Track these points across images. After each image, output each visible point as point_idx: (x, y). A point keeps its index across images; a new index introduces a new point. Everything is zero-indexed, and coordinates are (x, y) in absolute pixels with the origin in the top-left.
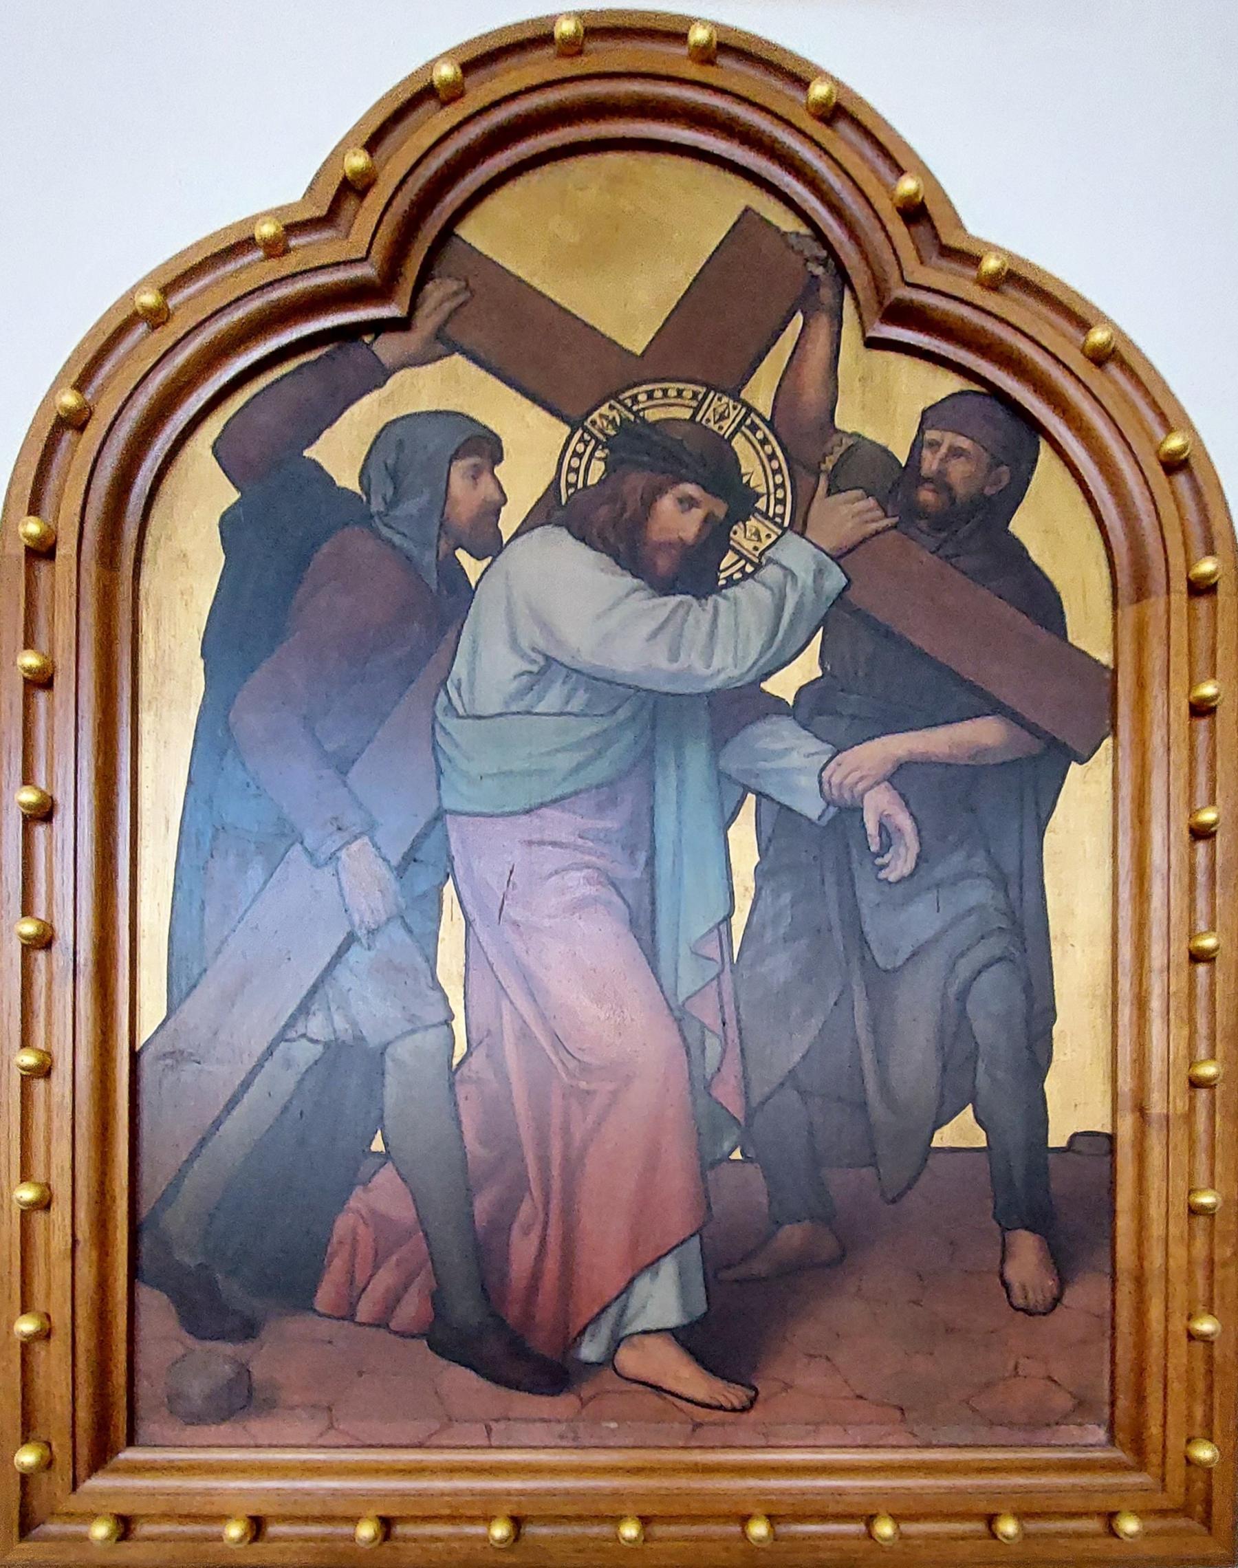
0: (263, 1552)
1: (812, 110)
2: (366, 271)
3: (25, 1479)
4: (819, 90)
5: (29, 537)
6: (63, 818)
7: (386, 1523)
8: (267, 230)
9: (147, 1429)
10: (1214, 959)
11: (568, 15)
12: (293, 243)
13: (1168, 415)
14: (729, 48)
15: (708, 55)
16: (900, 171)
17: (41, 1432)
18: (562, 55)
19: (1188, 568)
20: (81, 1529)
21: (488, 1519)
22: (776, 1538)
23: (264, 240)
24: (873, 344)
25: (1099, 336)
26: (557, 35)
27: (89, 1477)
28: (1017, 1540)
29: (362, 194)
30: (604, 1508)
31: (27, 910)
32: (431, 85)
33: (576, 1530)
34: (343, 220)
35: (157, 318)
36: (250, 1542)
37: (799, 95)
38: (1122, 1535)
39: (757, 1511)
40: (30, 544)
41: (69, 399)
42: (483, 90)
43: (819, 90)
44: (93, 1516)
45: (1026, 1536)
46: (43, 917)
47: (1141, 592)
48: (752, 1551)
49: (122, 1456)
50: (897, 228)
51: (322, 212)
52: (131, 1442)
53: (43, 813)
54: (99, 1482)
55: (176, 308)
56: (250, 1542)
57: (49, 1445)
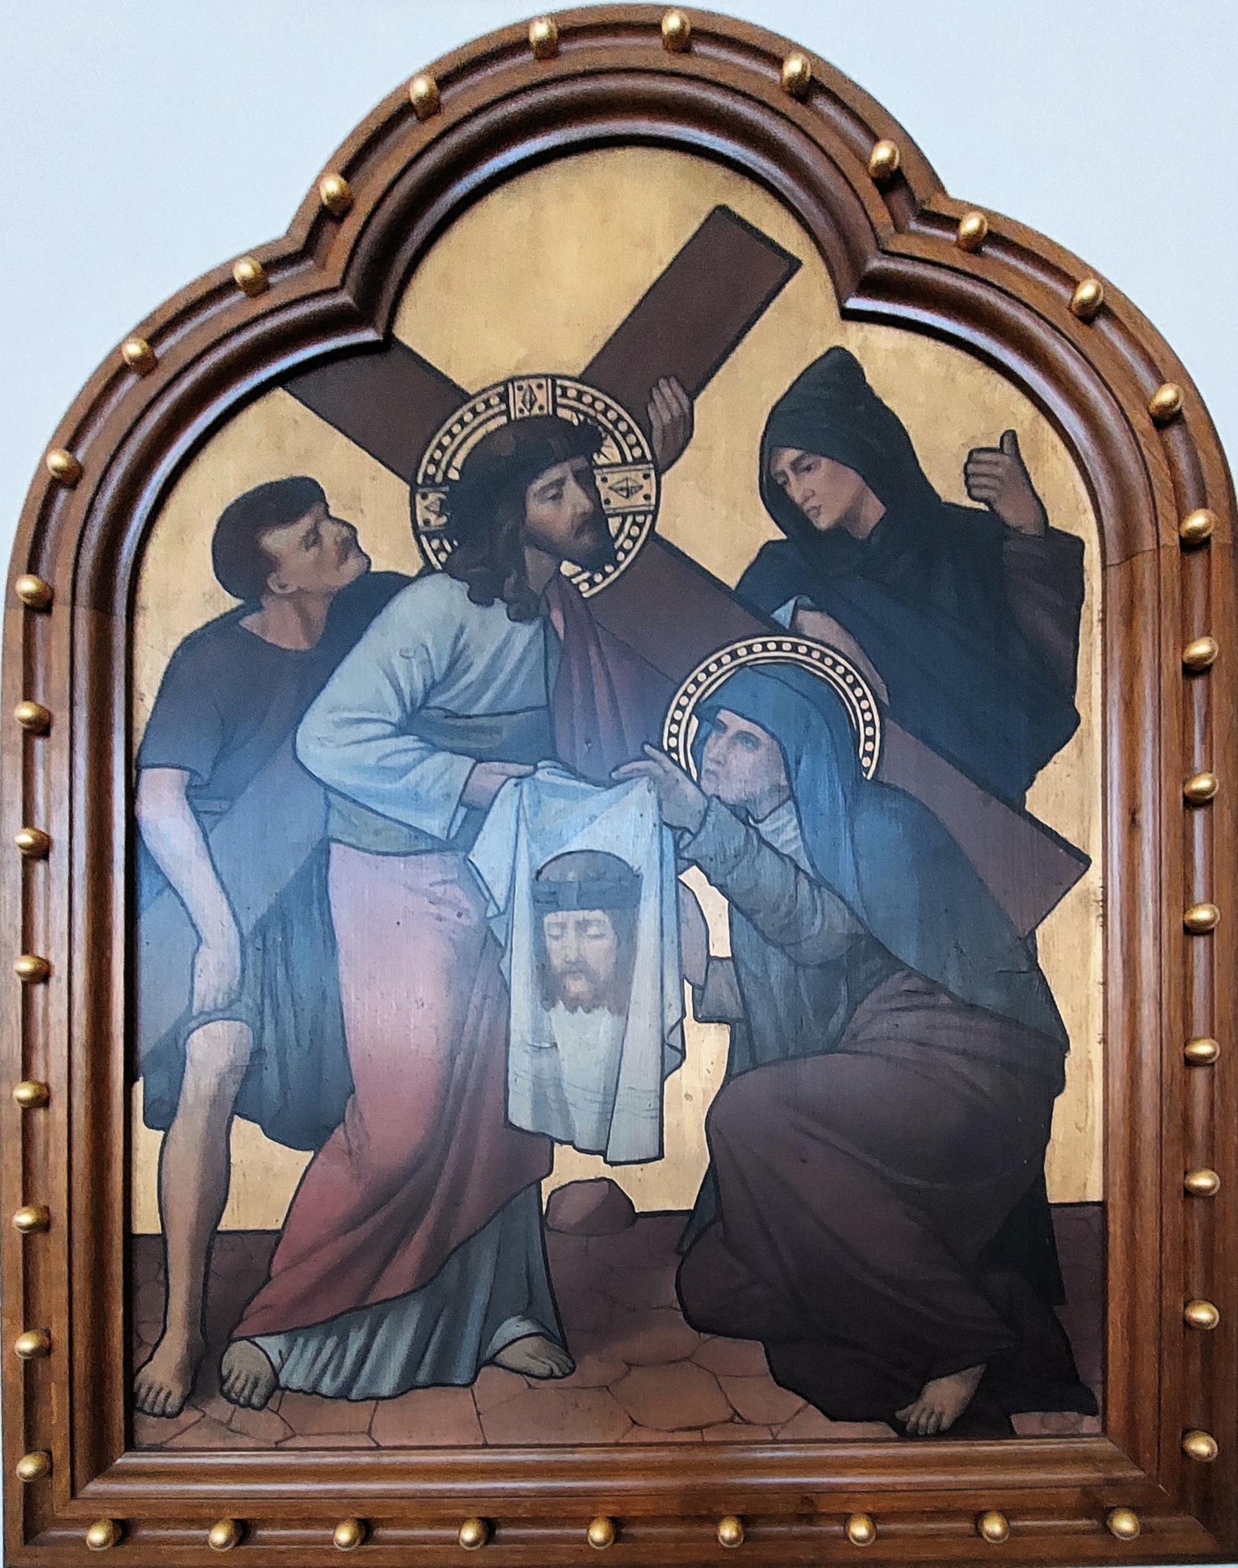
1: (788, 89)
2: (345, 298)
5: (27, 595)
6: (59, 856)
8: (244, 270)
10: (1212, 930)
11: (540, 18)
12: (272, 280)
14: (701, 33)
15: (682, 43)
17: (39, 1443)
20: (706, 1530)
22: (880, 1536)
24: (849, 315)
27: (88, 1482)
28: (1137, 1534)
31: (27, 949)
32: (410, 104)
34: (320, 249)
35: (145, 365)
36: (237, 1545)
37: (771, 73)
40: (28, 601)
42: (460, 99)
44: (90, 1522)
46: (41, 954)
49: (119, 1461)
52: (131, 1445)
54: (97, 1487)
55: (163, 357)
56: (237, 1545)
57: (50, 1453)
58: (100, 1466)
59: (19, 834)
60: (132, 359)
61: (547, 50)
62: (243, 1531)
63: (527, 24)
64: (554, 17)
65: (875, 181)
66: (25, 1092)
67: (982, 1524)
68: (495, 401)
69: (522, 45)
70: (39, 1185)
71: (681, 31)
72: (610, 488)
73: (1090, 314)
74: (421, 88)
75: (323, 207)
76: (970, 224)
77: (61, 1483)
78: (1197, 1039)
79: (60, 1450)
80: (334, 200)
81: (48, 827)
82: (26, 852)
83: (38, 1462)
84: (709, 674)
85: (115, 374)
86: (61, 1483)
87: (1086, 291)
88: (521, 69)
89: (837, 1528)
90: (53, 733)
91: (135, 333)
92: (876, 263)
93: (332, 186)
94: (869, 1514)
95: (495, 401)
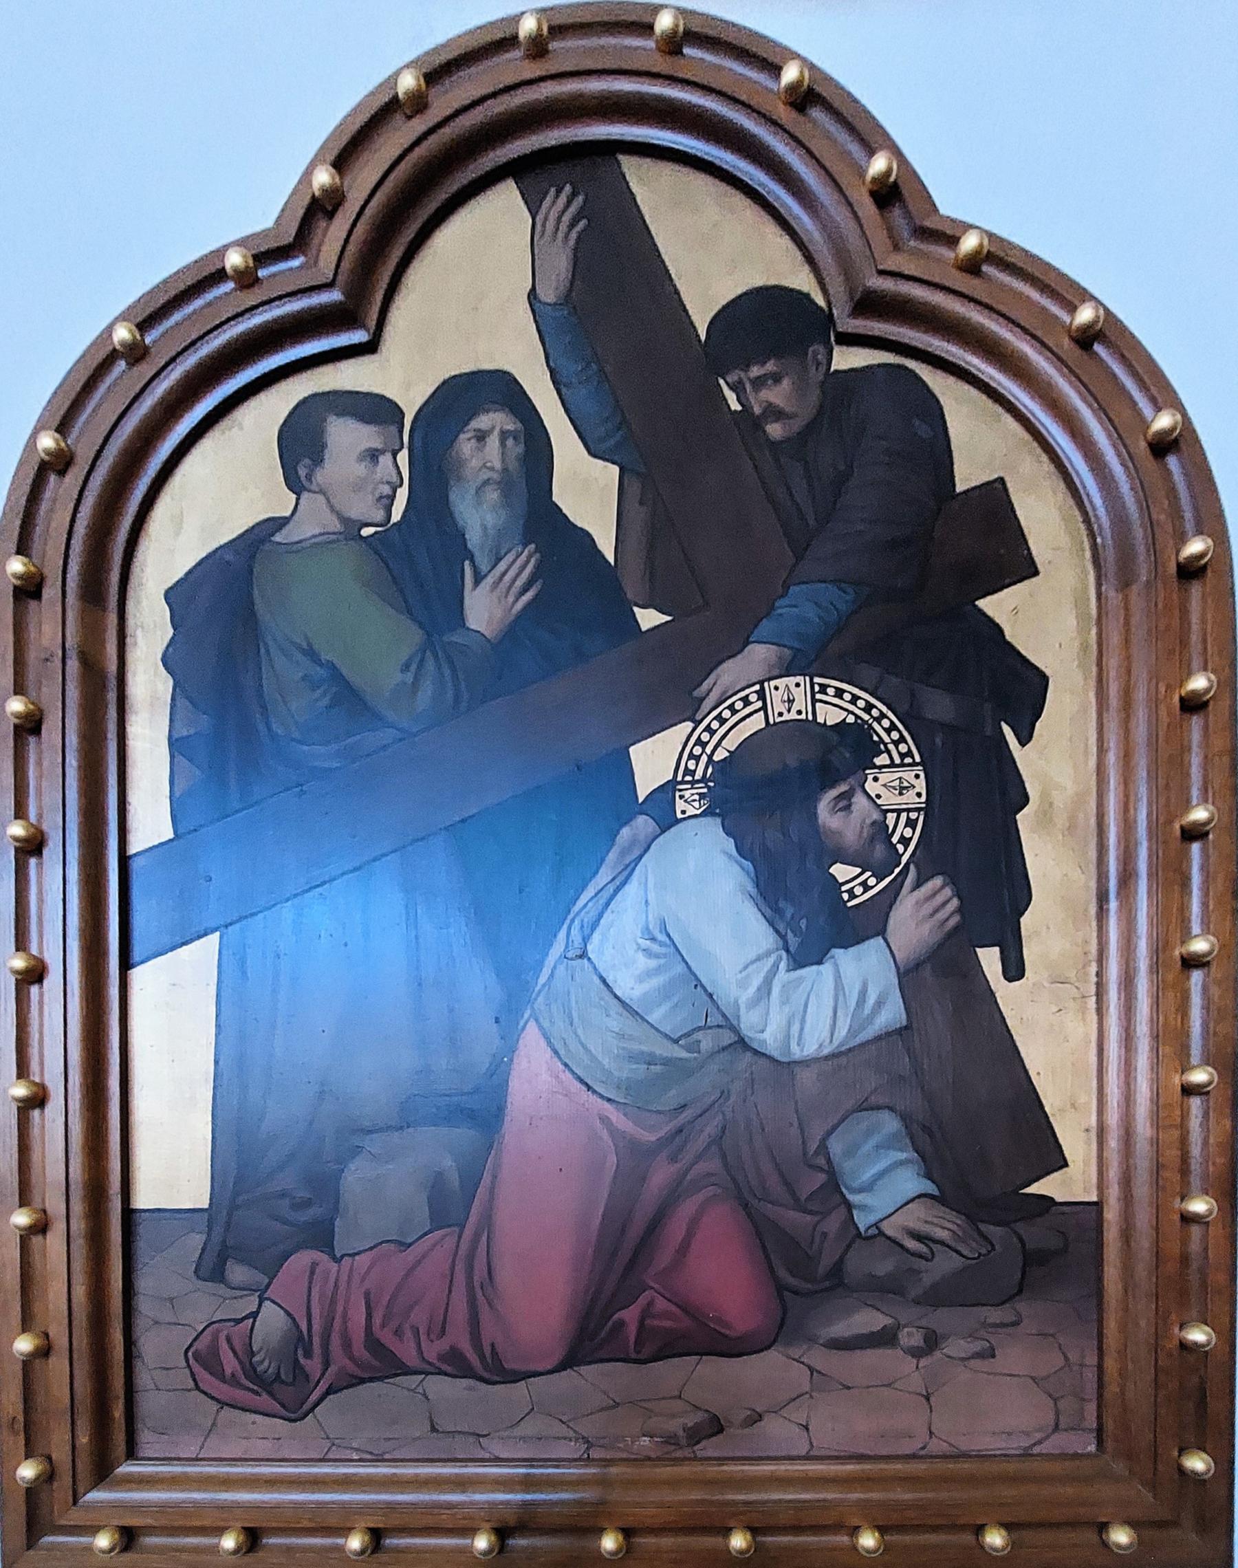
2: (335, 296)
3: (32, 1492)
5: (15, 576)
7: (376, 1536)
8: (234, 259)
9: (148, 1441)
12: (262, 273)
13: (1068, 293)
14: (700, 34)
16: (871, 152)
20: (213, 1541)
21: (471, 1531)
23: (236, 270)
29: (331, 215)
30: (333, 1521)
33: (933, 1538)
35: (135, 353)
40: (18, 583)
42: (444, 101)
43: (790, 74)
51: (289, 238)
52: (131, 1453)
53: (32, 847)
58: (102, 1473)
59: (13, 1085)
60: (123, 344)
61: (247, 280)
62: (252, 1538)
63: (516, 19)
65: (873, 194)
66: (22, 1218)
67: (983, 1536)
68: (753, 697)
69: (509, 42)
70: (37, 1307)
71: (674, 31)
72: (884, 785)
73: (1086, 338)
74: (408, 82)
75: (314, 199)
76: (969, 243)
77: (64, 1481)
78: (1194, 1067)
79: (61, 1455)
80: (324, 190)
81: (41, 952)
82: (19, 977)
83: (36, 1342)
84: (734, 712)
85: (209, 276)
86: (64, 1481)
87: (1085, 315)
89: (845, 1539)
90: (45, 852)
91: (123, 317)
93: (323, 177)
95: (753, 697)
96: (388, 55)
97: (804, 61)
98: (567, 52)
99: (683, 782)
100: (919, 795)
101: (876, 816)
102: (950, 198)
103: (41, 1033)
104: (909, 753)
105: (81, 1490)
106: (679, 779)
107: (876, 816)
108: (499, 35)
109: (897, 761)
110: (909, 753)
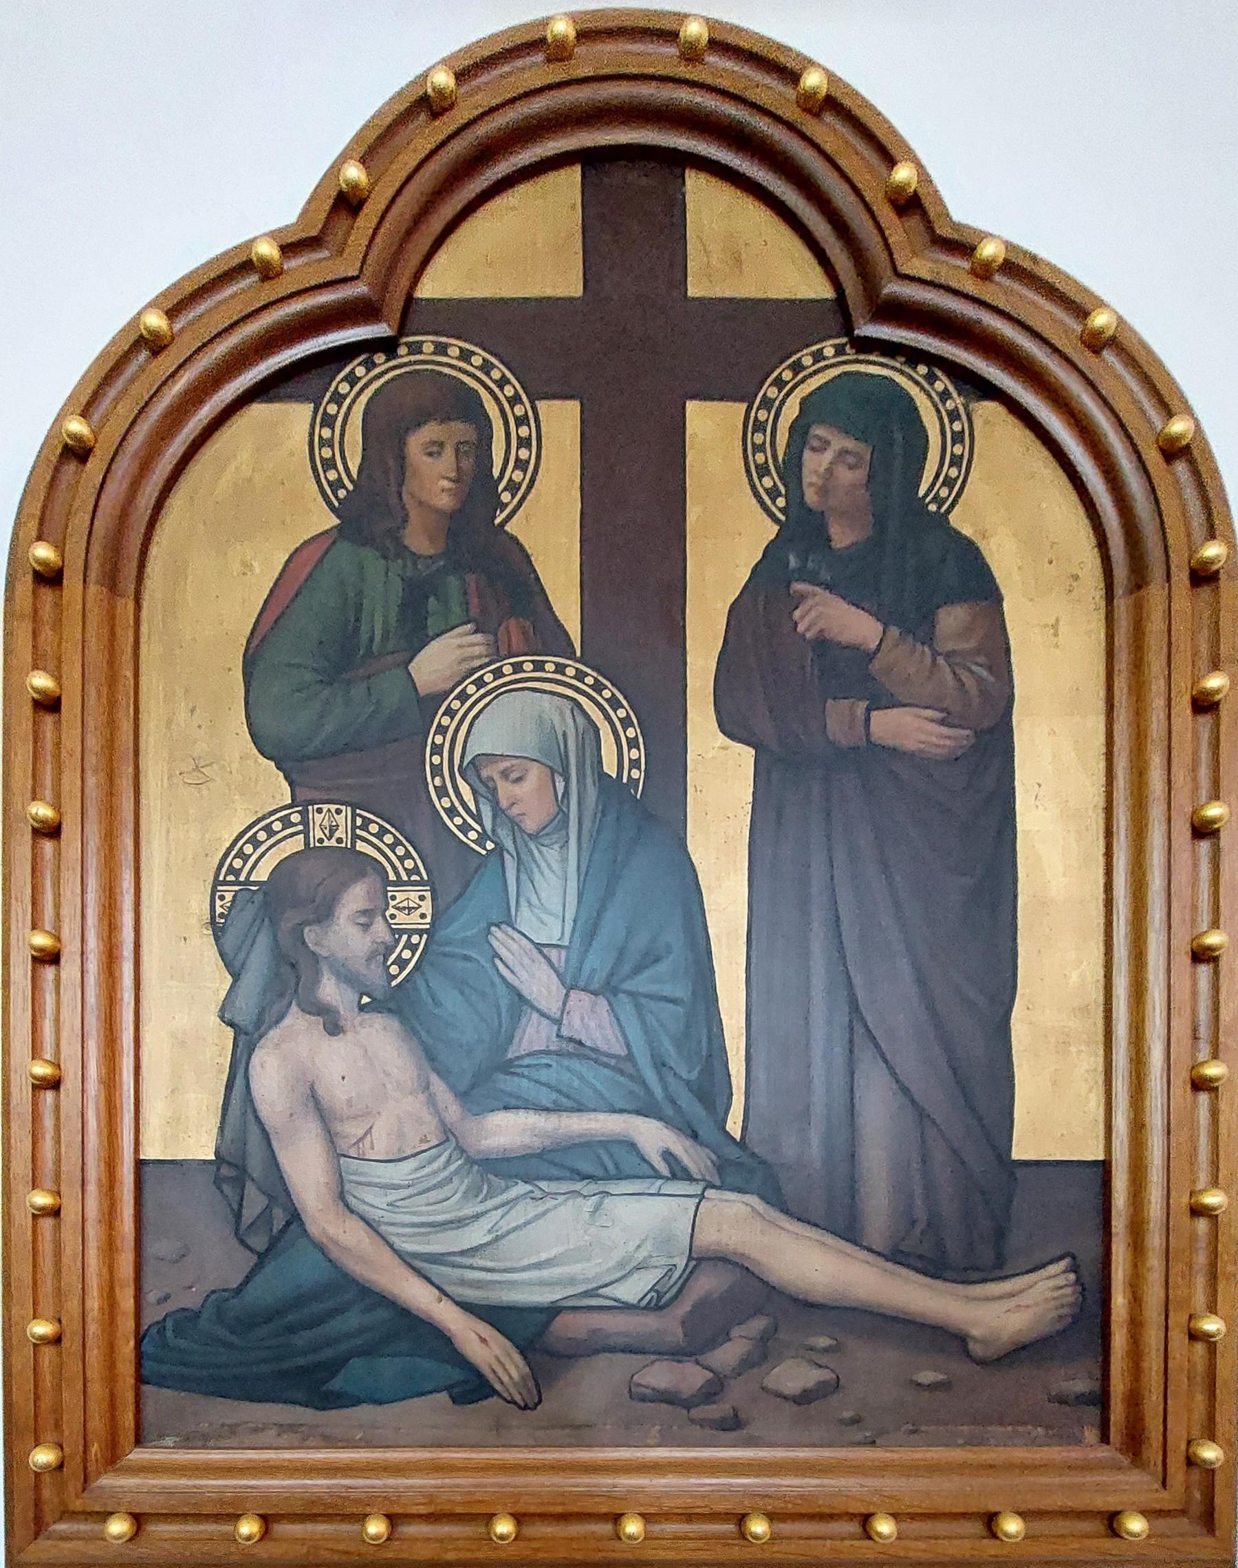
0: (141, 1551)
2: (360, 289)
4: (903, 174)
13: (1167, 400)
18: (973, 272)
19: (1195, 683)
20: (226, 1528)
25: (1178, 426)
26: (978, 253)
35: (558, 52)
38: (1000, 1535)
39: (498, 1509)
41: (156, 321)
43: (903, 174)
45: (774, 1538)
47: (1139, 580)
48: (619, 1552)
50: (886, 214)
52: (138, 1441)
54: (108, 1481)
58: (112, 1458)
61: (691, 54)
64: (574, 17)
77: (74, 1466)
85: (241, 266)
88: (662, 57)
92: (892, 288)
94: (511, 1514)
96: (420, 51)
97: (60, 419)
98: (588, 60)
99: (225, 883)
100: (423, 916)
101: (388, 938)
102: (963, 204)
103: (57, 1021)
104: (416, 870)
105: (92, 1475)
106: (221, 878)
107: (388, 938)
108: (527, 38)
109: (405, 878)
110: (416, 870)
